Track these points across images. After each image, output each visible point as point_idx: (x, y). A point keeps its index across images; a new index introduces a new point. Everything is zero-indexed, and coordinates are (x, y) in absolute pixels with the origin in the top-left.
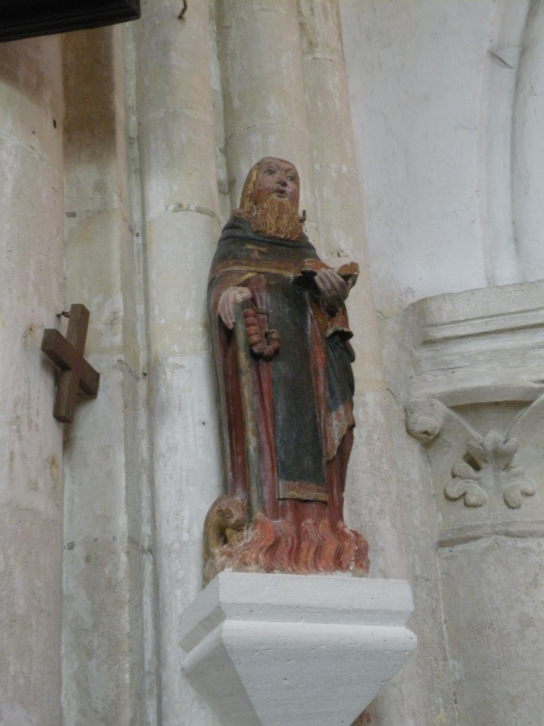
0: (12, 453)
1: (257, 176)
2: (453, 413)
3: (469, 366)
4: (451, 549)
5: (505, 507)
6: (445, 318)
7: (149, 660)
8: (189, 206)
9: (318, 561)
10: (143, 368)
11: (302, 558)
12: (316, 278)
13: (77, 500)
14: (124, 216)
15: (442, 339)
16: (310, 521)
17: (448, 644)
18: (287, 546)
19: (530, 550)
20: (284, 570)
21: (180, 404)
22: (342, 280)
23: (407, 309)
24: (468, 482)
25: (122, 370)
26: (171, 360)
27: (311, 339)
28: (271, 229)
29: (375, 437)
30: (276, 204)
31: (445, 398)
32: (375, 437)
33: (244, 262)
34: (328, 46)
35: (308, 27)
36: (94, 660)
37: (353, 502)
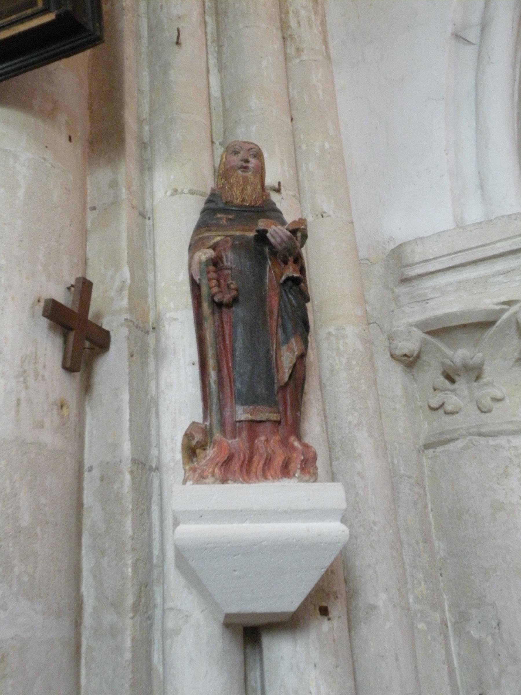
0: (19, 400)
1: (226, 158)
2: (429, 338)
3: (440, 297)
4: (434, 450)
5: (478, 412)
6: (417, 259)
7: (157, 556)
8: (183, 190)
9: (267, 471)
10: (153, 324)
11: (254, 469)
12: (268, 235)
13: (95, 432)
14: (132, 205)
15: (415, 276)
16: (263, 438)
17: (434, 528)
18: (239, 461)
19: (502, 447)
20: (236, 480)
21: (175, 350)
22: (289, 233)
23: (389, 255)
24: (446, 394)
25: (128, 326)
26: (168, 315)
27: (268, 286)
28: (237, 199)
29: (354, 363)
30: (241, 178)
31: (420, 325)
32: (354, 363)
33: (213, 228)
34: (312, 49)
35: (296, 37)
36: (106, 558)
37: (336, 418)
